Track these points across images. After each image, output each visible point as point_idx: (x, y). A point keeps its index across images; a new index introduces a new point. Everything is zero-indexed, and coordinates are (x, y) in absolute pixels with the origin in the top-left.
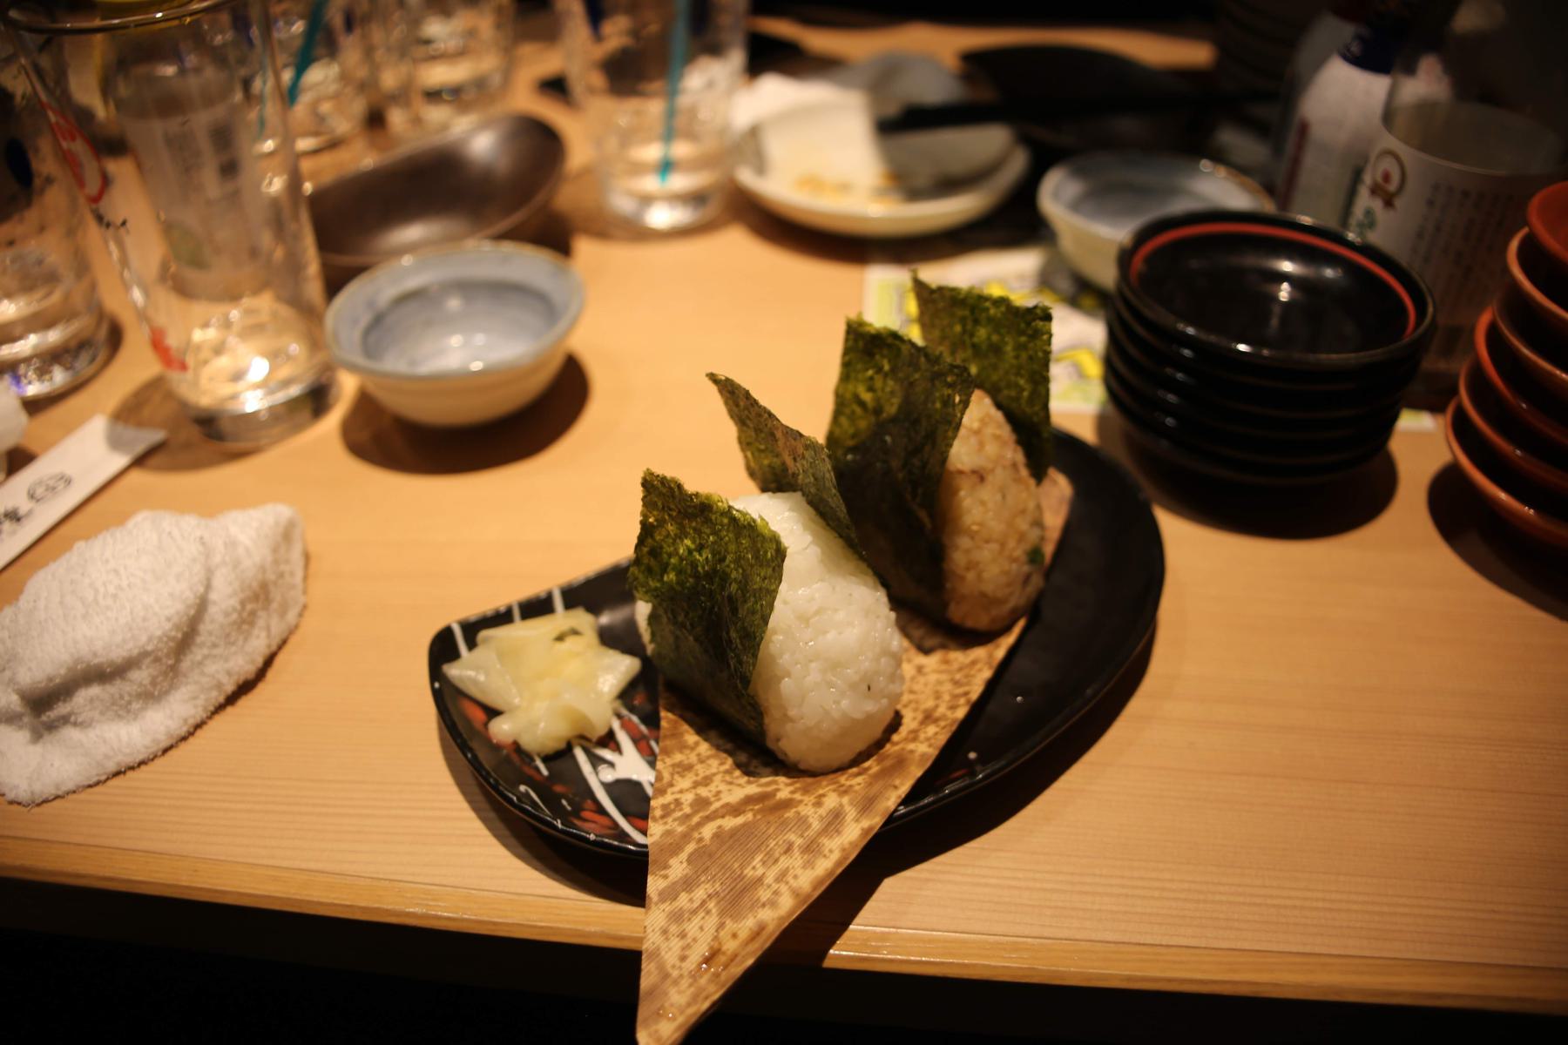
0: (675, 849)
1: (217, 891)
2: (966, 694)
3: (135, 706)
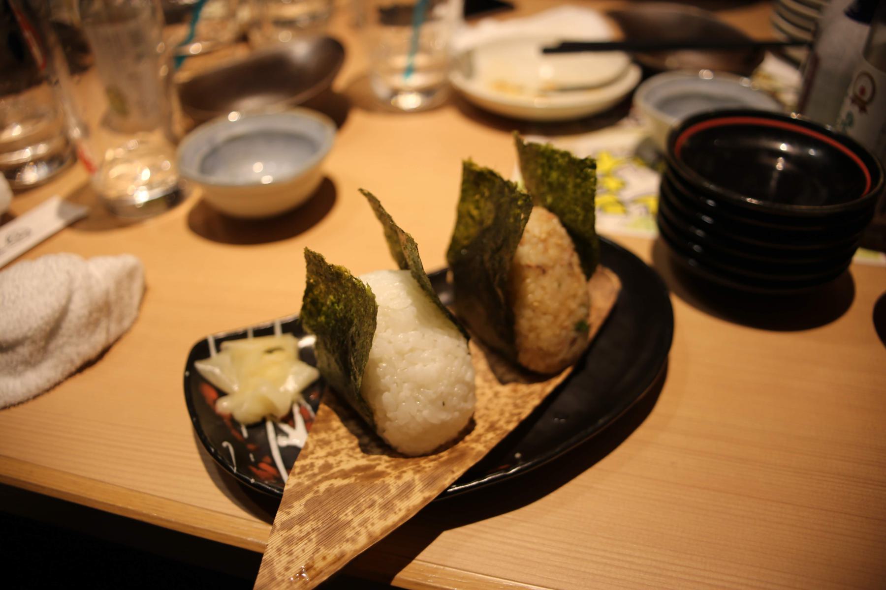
0: (299, 495)
1: (39, 486)
2: (519, 414)
3: (20, 368)
